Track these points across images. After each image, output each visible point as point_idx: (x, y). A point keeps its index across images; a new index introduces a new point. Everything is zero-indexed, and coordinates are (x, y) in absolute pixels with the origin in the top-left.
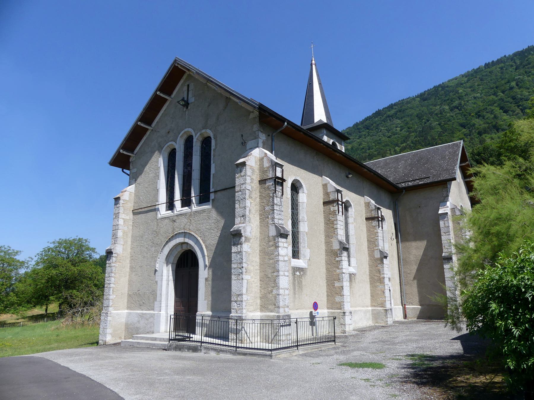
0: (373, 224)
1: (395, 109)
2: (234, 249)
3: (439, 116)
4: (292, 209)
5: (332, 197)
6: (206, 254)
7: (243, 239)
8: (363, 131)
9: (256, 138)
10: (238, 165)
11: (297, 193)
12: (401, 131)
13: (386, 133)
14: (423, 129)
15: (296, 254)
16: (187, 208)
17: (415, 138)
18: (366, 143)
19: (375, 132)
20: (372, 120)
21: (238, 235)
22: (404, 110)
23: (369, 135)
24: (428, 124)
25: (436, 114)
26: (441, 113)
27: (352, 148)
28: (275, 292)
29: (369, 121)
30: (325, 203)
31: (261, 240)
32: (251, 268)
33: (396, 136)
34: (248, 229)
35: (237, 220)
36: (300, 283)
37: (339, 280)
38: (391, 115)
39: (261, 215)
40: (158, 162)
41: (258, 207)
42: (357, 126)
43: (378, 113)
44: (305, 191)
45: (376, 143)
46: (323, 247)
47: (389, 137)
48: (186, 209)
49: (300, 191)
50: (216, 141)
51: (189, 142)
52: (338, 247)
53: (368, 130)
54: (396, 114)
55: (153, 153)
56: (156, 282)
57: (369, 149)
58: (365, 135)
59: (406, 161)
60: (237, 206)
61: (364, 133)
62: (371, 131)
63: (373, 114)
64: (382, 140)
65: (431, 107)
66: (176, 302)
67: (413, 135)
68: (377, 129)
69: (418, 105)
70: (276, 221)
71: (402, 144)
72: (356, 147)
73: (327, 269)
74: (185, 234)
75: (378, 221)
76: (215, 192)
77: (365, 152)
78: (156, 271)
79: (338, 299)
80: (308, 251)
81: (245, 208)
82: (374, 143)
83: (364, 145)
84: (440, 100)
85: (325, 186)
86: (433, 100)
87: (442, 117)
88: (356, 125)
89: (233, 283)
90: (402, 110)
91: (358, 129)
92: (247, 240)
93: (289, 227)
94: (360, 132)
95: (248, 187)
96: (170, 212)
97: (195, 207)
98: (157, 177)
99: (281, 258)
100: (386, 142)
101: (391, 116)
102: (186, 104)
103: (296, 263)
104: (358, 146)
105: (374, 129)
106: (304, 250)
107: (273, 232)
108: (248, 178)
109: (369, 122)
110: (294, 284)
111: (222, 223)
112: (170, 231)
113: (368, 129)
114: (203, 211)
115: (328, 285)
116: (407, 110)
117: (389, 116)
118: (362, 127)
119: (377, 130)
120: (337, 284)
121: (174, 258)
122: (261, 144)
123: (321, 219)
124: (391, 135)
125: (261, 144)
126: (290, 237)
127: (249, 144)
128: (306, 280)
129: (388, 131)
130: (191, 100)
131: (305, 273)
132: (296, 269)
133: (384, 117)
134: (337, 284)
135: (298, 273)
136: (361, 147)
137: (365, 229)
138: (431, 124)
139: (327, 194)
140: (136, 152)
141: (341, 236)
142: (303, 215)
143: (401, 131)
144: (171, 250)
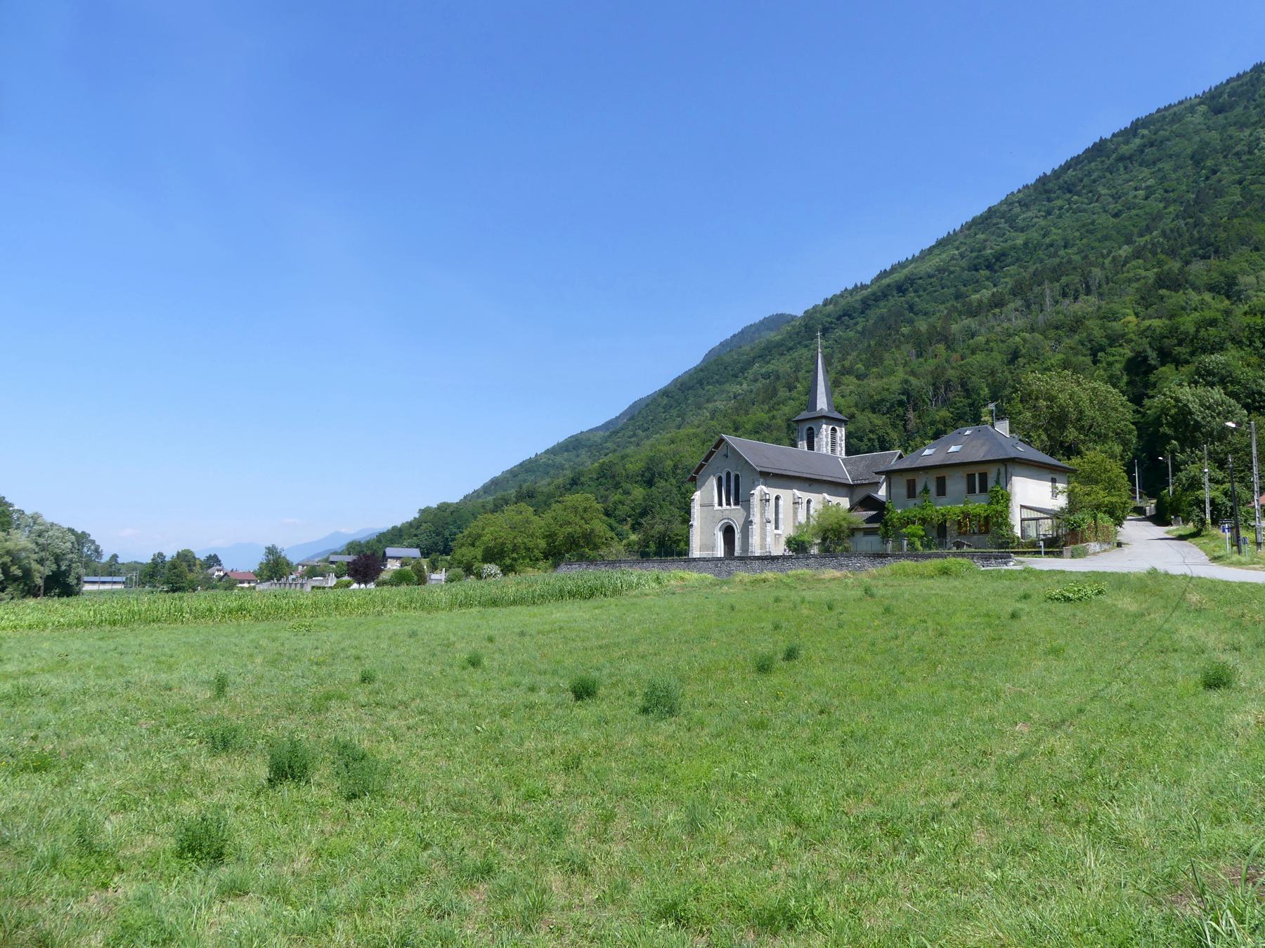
1: (1143, 136)
3: (1244, 158)
8: (1058, 198)
12: (1146, 198)
13: (1109, 203)
14: (1197, 196)
15: (777, 528)
17: (1173, 220)
18: (1060, 231)
19: (1086, 201)
20: (1080, 169)
21: (751, 522)
22: (1161, 142)
23: (1071, 208)
24: (1214, 178)
25: (1237, 154)
26: (1250, 153)
27: (1026, 244)
29: (1075, 170)
33: (1134, 212)
38: (1127, 154)
42: (1044, 184)
43: (1099, 149)
45: (1083, 230)
46: (792, 524)
47: (1116, 215)
48: (728, 507)
51: (728, 474)
53: (1068, 196)
54: (1142, 151)
55: (710, 476)
57: (1065, 247)
58: (1061, 208)
61: (1059, 203)
62: (1076, 197)
63: (1087, 151)
64: (1099, 224)
65: (1232, 131)
67: (1170, 213)
68: (1091, 192)
69: (1199, 127)
71: (1142, 236)
72: (1036, 242)
74: (728, 519)
77: (1055, 255)
82: (1078, 230)
83: (1055, 237)
84: (1258, 109)
86: (1239, 110)
87: (1249, 163)
88: (1043, 180)
90: (1156, 140)
91: (1047, 191)
94: (1049, 200)
97: (733, 507)
100: (1107, 228)
101: (1130, 158)
103: (776, 532)
104: (1040, 238)
105: (1084, 191)
107: (765, 521)
109: (1074, 173)
113: (1070, 192)
116: (1168, 140)
117: (1121, 159)
118: (1057, 188)
119: (1090, 195)
124: (1120, 211)
127: (756, 483)
129: (1116, 198)
130: (729, 455)
133: (1111, 160)
136: (1047, 240)
138: (1220, 181)
142: (781, 510)
143: (1146, 198)
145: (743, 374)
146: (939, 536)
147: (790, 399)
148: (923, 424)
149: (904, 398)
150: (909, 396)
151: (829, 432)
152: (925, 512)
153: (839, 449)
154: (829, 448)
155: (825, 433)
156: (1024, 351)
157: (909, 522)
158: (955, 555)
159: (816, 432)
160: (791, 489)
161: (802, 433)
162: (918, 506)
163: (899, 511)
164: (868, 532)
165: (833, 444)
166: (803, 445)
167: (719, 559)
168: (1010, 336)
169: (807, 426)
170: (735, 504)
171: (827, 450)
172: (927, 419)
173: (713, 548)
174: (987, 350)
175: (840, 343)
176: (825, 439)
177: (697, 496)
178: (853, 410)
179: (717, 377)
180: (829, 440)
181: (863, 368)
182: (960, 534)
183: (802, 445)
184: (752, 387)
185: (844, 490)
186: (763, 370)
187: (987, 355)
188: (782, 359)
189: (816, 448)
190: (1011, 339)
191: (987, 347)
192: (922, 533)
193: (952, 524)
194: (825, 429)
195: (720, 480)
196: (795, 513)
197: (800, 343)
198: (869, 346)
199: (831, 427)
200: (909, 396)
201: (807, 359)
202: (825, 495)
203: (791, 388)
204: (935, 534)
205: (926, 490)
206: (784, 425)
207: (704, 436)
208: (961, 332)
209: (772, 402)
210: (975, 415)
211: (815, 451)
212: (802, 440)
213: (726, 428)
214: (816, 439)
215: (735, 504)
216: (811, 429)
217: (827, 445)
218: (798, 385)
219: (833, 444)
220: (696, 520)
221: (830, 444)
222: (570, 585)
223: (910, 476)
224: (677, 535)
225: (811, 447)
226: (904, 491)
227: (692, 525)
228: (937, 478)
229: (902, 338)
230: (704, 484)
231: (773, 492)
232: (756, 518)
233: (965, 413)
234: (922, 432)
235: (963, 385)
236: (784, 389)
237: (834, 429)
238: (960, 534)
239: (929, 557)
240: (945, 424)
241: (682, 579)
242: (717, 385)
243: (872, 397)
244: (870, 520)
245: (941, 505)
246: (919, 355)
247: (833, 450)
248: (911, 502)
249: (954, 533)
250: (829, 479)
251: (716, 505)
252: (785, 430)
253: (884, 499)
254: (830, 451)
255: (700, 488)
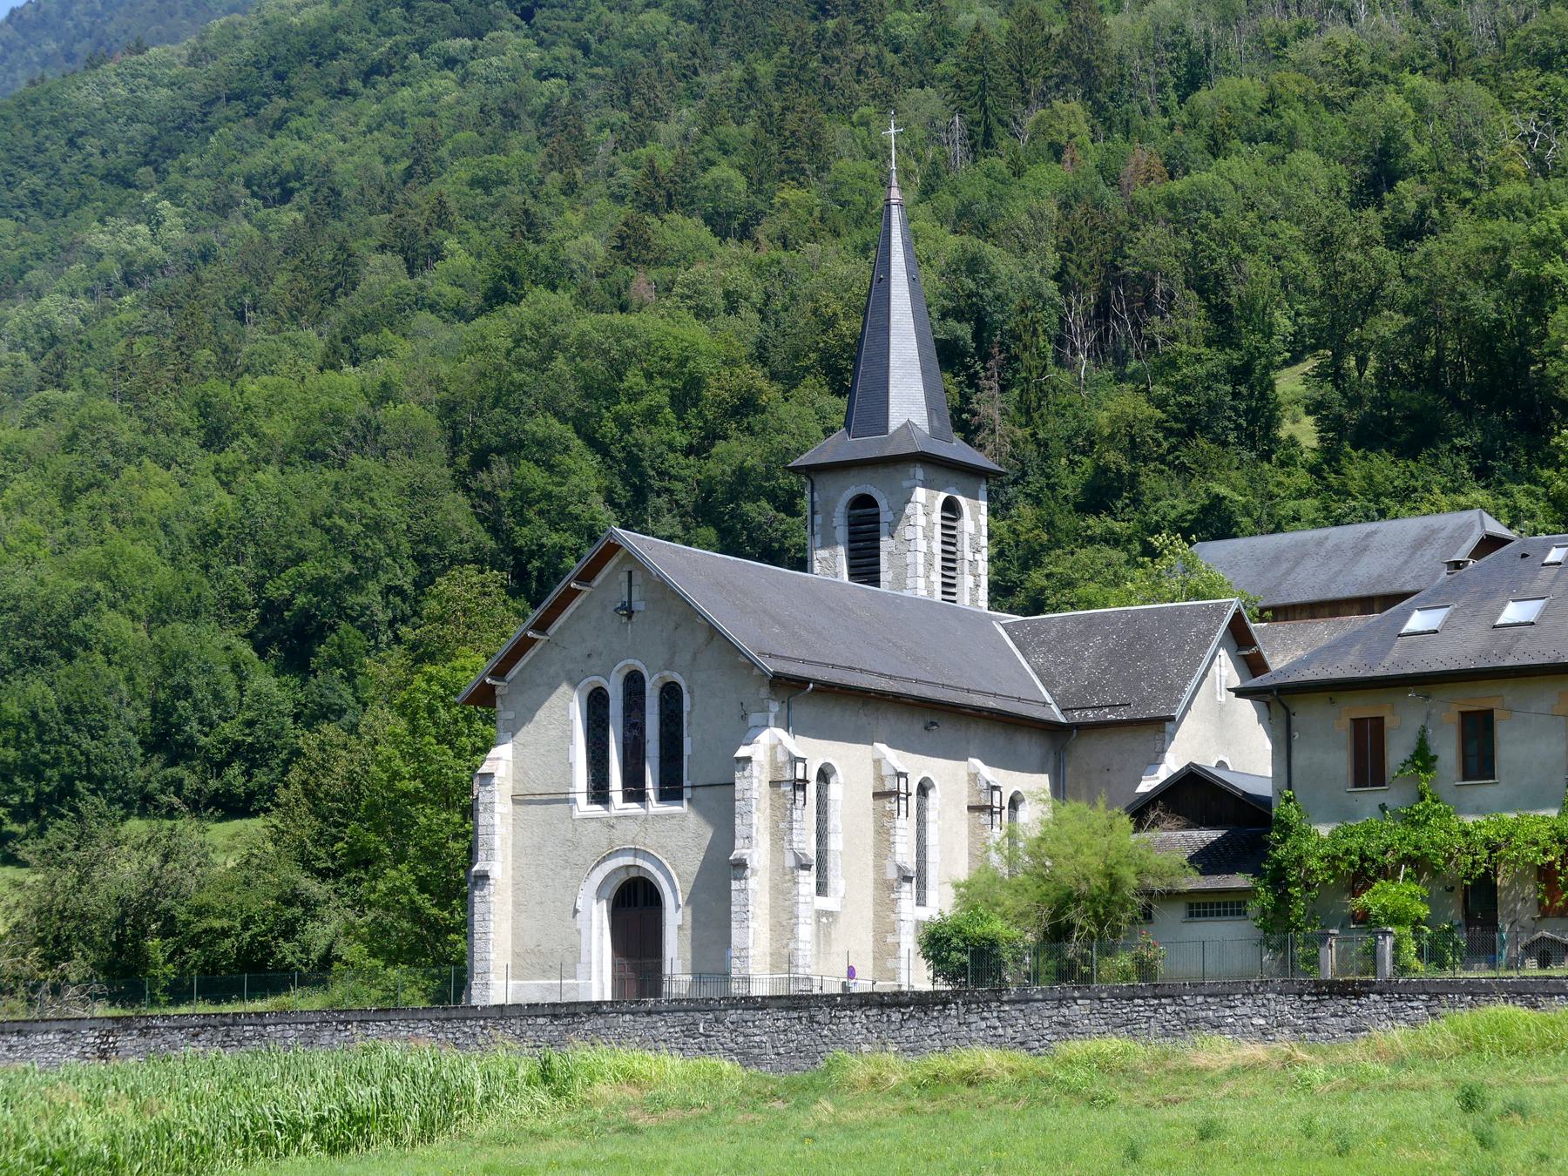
0: (982, 821)
2: (735, 885)
4: (818, 812)
5: (890, 785)
6: (678, 886)
7: (748, 872)
9: (765, 710)
10: (739, 760)
11: (827, 782)
15: (822, 889)
16: (635, 805)
21: (741, 865)
28: (792, 945)
30: (877, 795)
31: (772, 872)
32: (758, 912)
34: (755, 857)
35: (739, 843)
36: (828, 935)
37: (894, 931)
39: (772, 834)
40: (567, 709)
41: (768, 823)
44: (841, 779)
46: (870, 875)
48: (634, 808)
49: (832, 780)
50: (692, 697)
51: (634, 683)
52: (895, 876)
55: (553, 688)
56: (579, 932)
59: (1106, 637)
60: (738, 821)
66: (614, 965)
70: (795, 845)
73: (876, 914)
74: (636, 852)
75: (992, 813)
76: (693, 787)
78: (576, 911)
79: (890, 964)
80: (842, 882)
81: (751, 825)
85: (877, 763)
89: (734, 932)
92: (754, 872)
93: (811, 850)
95: (755, 795)
96: (599, 807)
97: (655, 806)
98: (571, 739)
99: (801, 899)
102: (628, 611)
103: (822, 903)
106: (836, 880)
107: (790, 861)
108: (755, 781)
110: (818, 936)
111: (708, 833)
112: (604, 843)
114: (672, 816)
115: (876, 940)
120: (890, 939)
121: (610, 891)
122: (772, 721)
123: (868, 825)
125: (772, 721)
126: (814, 868)
127: (754, 718)
128: (838, 932)
130: (638, 605)
131: (835, 920)
132: (820, 914)
134: (890, 939)
135: (824, 920)
137: (964, 830)
139: (880, 778)
140: (509, 677)
141: (905, 852)
142: (835, 820)
144: (607, 877)
145: (161, 174)
146: (1469, 920)
147: (421, 303)
148: (1042, 445)
149: (964, 331)
150: (982, 328)
151: (937, 516)
152: (1423, 836)
153: (969, 581)
154: (937, 578)
155: (921, 520)
156: (1419, 151)
157: (1362, 875)
158: (1524, 993)
159: (885, 516)
160: (961, 756)
161: (829, 515)
162: (1397, 815)
163: (1324, 831)
164: (1202, 906)
165: (950, 561)
166: (831, 563)
167: (595, 1008)
168: (1360, 82)
169: (852, 492)
170: (664, 796)
171: (929, 584)
172: (1054, 428)
173: (568, 961)
174: (1270, 137)
175: (605, 60)
176: (922, 545)
177: (502, 760)
178: (756, 377)
179: (36, 181)
180: (937, 547)
181: (740, 183)
182: (1545, 912)
183: (830, 565)
184: (211, 236)
185: (1030, 746)
186: (259, 160)
187: (1272, 161)
188: (341, 115)
189: (886, 575)
190: (1368, 97)
191: (1271, 124)
192: (1423, 911)
193: (1519, 878)
194: (925, 503)
195: (596, 705)
196: (884, 834)
197: (420, 47)
198: (751, 82)
199: (942, 496)
200: (982, 328)
201: (460, 122)
202: (976, 763)
203: (418, 256)
204: (1455, 913)
205: (1423, 758)
206: (428, 421)
207: (65, 463)
208: (1145, 50)
209: (336, 317)
210: (1253, 414)
211: (884, 587)
212: (828, 543)
213: (168, 430)
214: (886, 544)
215: (664, 796)
216: (864, 502)
217: (929, 564)
218: (451, 244)
219: (950, 561)
220: (498, 855)
221: (938, 563)
222: (307, 1101)
223: (1365, 707)
224: (201, 911)
225: (865, 567)
226: (1339, 760)
227: (484, 877)
228: (1463, 714)
229: (890, 58)
230: (528, 714)
231: (815, 752)
232: (757, 849)
233: (1214, 408)
234: (1036, 481)
235: (1205, 284)
236: (388, 257)
237: (950, 507)
238: (1545, 912)
239: (1435, 993)
240: (1134, 449)
241: (631, 1079)
242: (36, 218)
243: (829, 323)
244: (1206, 860)
245: (1478, 811)
246: (981, 141)
247: (948, 587)
248: (1370, 799)
249: (1526, 913)
250: (991, 703)
251: (582, 799)
252: (441, 452)
253: (1265, 789)
254: (938, 588)
255: (513, 730)
